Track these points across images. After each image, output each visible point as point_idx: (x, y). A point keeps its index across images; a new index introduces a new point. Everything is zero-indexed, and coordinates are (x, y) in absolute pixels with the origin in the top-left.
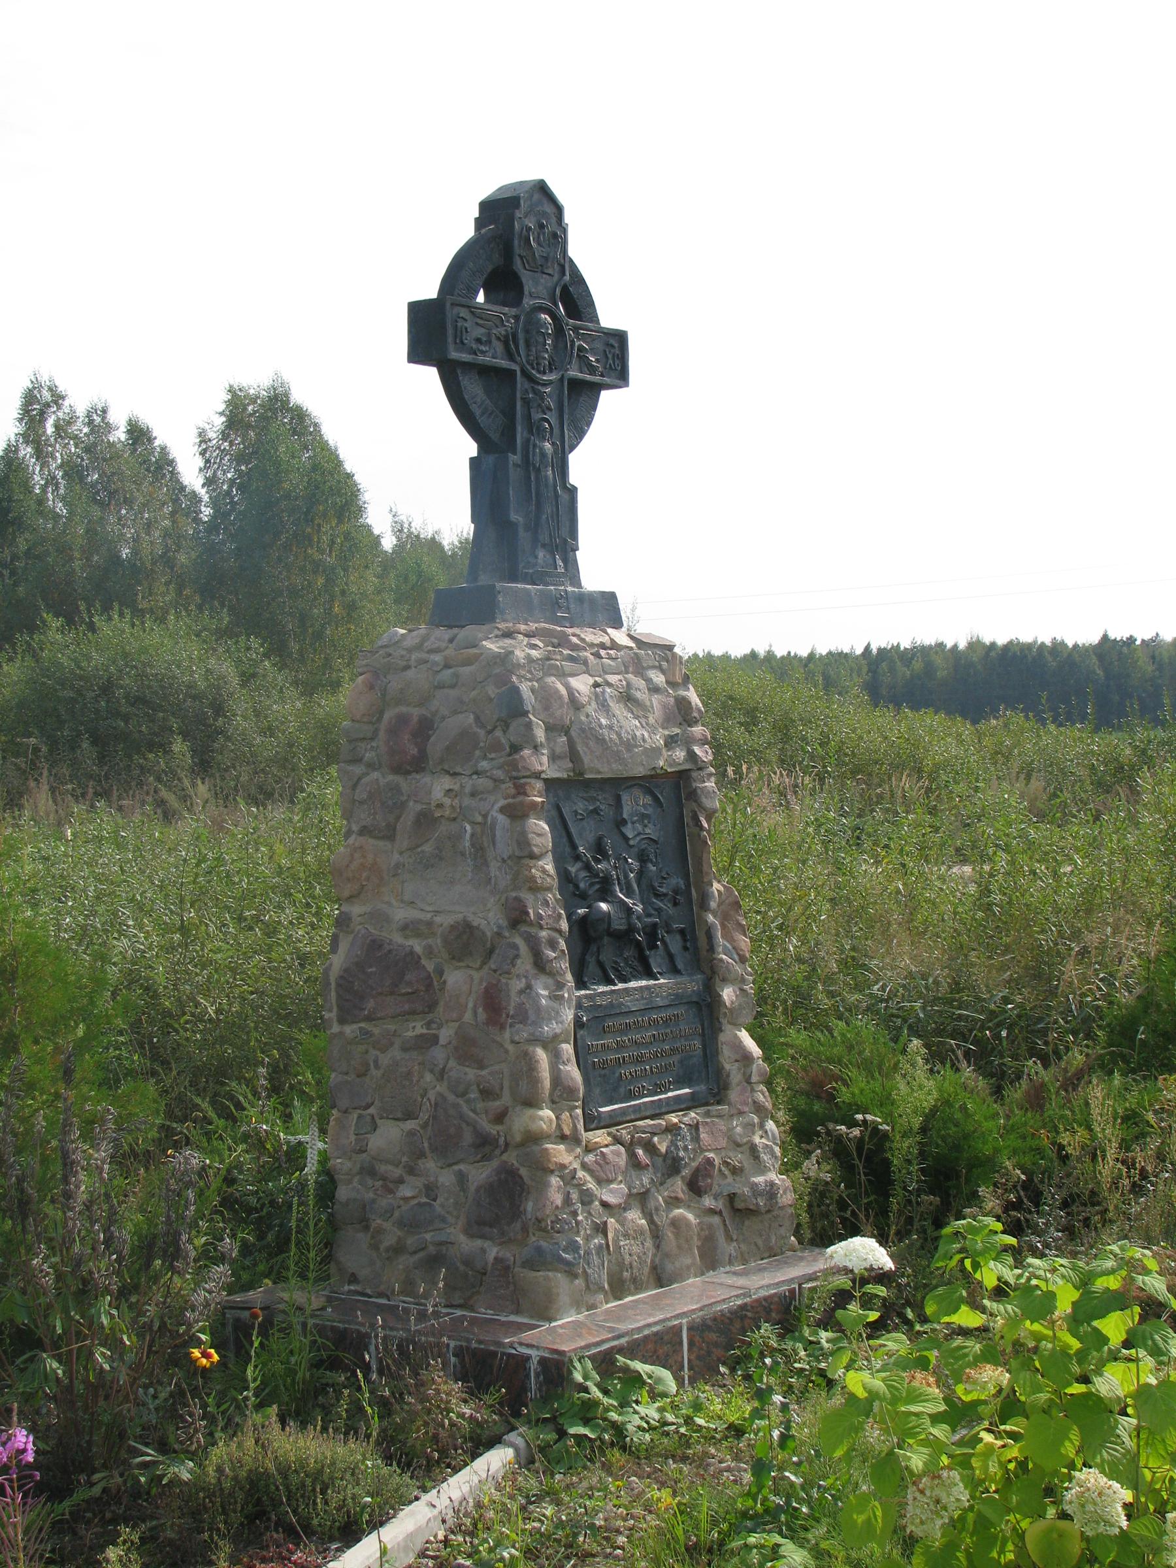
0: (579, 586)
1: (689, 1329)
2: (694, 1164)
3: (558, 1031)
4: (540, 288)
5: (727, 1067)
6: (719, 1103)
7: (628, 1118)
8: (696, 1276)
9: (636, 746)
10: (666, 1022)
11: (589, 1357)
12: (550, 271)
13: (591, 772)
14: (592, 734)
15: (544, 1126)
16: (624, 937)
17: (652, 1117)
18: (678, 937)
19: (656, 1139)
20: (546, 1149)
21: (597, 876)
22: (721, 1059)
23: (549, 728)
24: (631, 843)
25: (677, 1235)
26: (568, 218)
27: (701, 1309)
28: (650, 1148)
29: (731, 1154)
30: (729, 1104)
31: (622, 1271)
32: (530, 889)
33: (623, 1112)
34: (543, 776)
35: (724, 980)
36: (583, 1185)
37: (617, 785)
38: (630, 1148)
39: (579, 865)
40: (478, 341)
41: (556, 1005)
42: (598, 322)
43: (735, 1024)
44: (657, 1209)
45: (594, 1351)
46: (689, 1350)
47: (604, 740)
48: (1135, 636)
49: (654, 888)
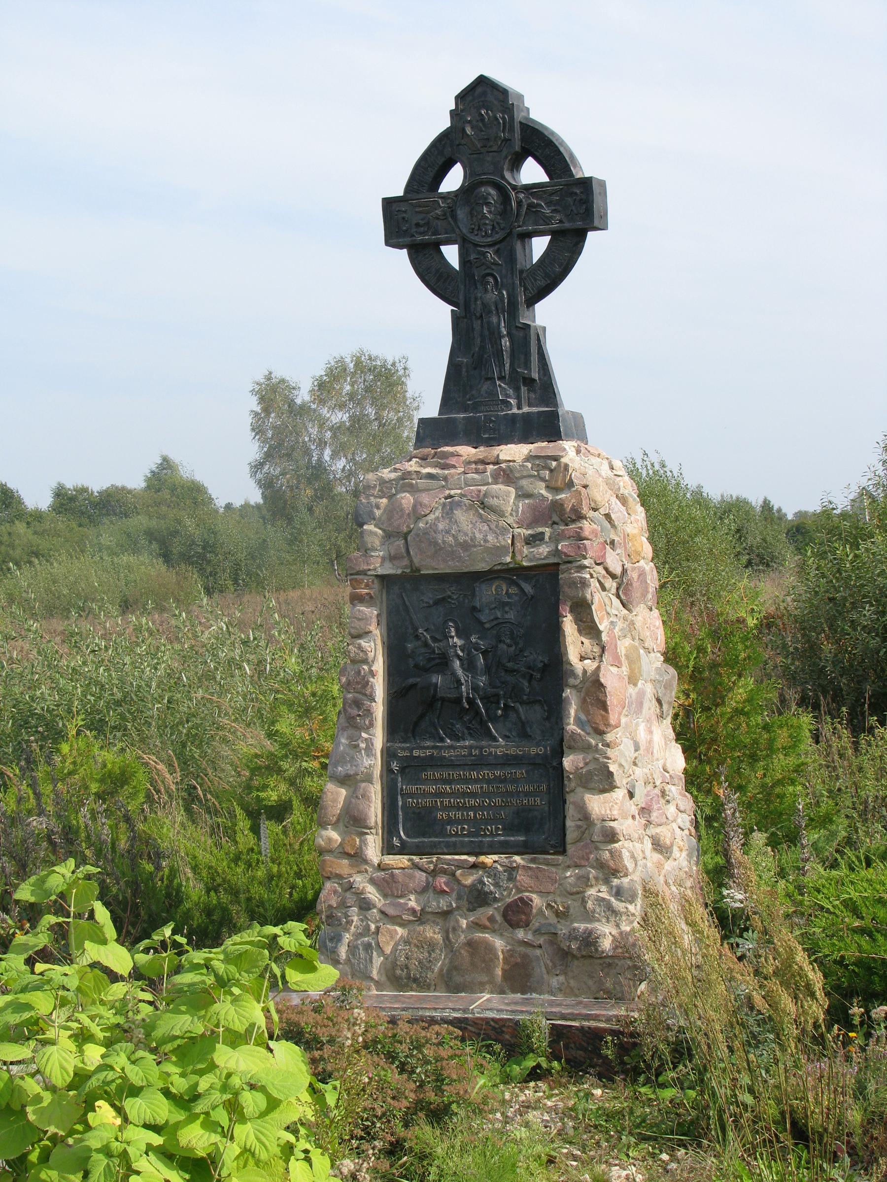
2: (509, 900)
7: (439, 851)
9: (475, 546)
10: (502, 780)
13: (428, 569)
14: (427, 538)
19: (459, 872)
20: (324, 861)
21: (434, 651)
23: (388, 536)
25: (472, 955)
29: (558, 899)
33: (434, 845)
34: (370, 573)
36: (362, 893)
40: (417, 225)
41: (351, 752)
43: (585, 787)
47: (436, 544)
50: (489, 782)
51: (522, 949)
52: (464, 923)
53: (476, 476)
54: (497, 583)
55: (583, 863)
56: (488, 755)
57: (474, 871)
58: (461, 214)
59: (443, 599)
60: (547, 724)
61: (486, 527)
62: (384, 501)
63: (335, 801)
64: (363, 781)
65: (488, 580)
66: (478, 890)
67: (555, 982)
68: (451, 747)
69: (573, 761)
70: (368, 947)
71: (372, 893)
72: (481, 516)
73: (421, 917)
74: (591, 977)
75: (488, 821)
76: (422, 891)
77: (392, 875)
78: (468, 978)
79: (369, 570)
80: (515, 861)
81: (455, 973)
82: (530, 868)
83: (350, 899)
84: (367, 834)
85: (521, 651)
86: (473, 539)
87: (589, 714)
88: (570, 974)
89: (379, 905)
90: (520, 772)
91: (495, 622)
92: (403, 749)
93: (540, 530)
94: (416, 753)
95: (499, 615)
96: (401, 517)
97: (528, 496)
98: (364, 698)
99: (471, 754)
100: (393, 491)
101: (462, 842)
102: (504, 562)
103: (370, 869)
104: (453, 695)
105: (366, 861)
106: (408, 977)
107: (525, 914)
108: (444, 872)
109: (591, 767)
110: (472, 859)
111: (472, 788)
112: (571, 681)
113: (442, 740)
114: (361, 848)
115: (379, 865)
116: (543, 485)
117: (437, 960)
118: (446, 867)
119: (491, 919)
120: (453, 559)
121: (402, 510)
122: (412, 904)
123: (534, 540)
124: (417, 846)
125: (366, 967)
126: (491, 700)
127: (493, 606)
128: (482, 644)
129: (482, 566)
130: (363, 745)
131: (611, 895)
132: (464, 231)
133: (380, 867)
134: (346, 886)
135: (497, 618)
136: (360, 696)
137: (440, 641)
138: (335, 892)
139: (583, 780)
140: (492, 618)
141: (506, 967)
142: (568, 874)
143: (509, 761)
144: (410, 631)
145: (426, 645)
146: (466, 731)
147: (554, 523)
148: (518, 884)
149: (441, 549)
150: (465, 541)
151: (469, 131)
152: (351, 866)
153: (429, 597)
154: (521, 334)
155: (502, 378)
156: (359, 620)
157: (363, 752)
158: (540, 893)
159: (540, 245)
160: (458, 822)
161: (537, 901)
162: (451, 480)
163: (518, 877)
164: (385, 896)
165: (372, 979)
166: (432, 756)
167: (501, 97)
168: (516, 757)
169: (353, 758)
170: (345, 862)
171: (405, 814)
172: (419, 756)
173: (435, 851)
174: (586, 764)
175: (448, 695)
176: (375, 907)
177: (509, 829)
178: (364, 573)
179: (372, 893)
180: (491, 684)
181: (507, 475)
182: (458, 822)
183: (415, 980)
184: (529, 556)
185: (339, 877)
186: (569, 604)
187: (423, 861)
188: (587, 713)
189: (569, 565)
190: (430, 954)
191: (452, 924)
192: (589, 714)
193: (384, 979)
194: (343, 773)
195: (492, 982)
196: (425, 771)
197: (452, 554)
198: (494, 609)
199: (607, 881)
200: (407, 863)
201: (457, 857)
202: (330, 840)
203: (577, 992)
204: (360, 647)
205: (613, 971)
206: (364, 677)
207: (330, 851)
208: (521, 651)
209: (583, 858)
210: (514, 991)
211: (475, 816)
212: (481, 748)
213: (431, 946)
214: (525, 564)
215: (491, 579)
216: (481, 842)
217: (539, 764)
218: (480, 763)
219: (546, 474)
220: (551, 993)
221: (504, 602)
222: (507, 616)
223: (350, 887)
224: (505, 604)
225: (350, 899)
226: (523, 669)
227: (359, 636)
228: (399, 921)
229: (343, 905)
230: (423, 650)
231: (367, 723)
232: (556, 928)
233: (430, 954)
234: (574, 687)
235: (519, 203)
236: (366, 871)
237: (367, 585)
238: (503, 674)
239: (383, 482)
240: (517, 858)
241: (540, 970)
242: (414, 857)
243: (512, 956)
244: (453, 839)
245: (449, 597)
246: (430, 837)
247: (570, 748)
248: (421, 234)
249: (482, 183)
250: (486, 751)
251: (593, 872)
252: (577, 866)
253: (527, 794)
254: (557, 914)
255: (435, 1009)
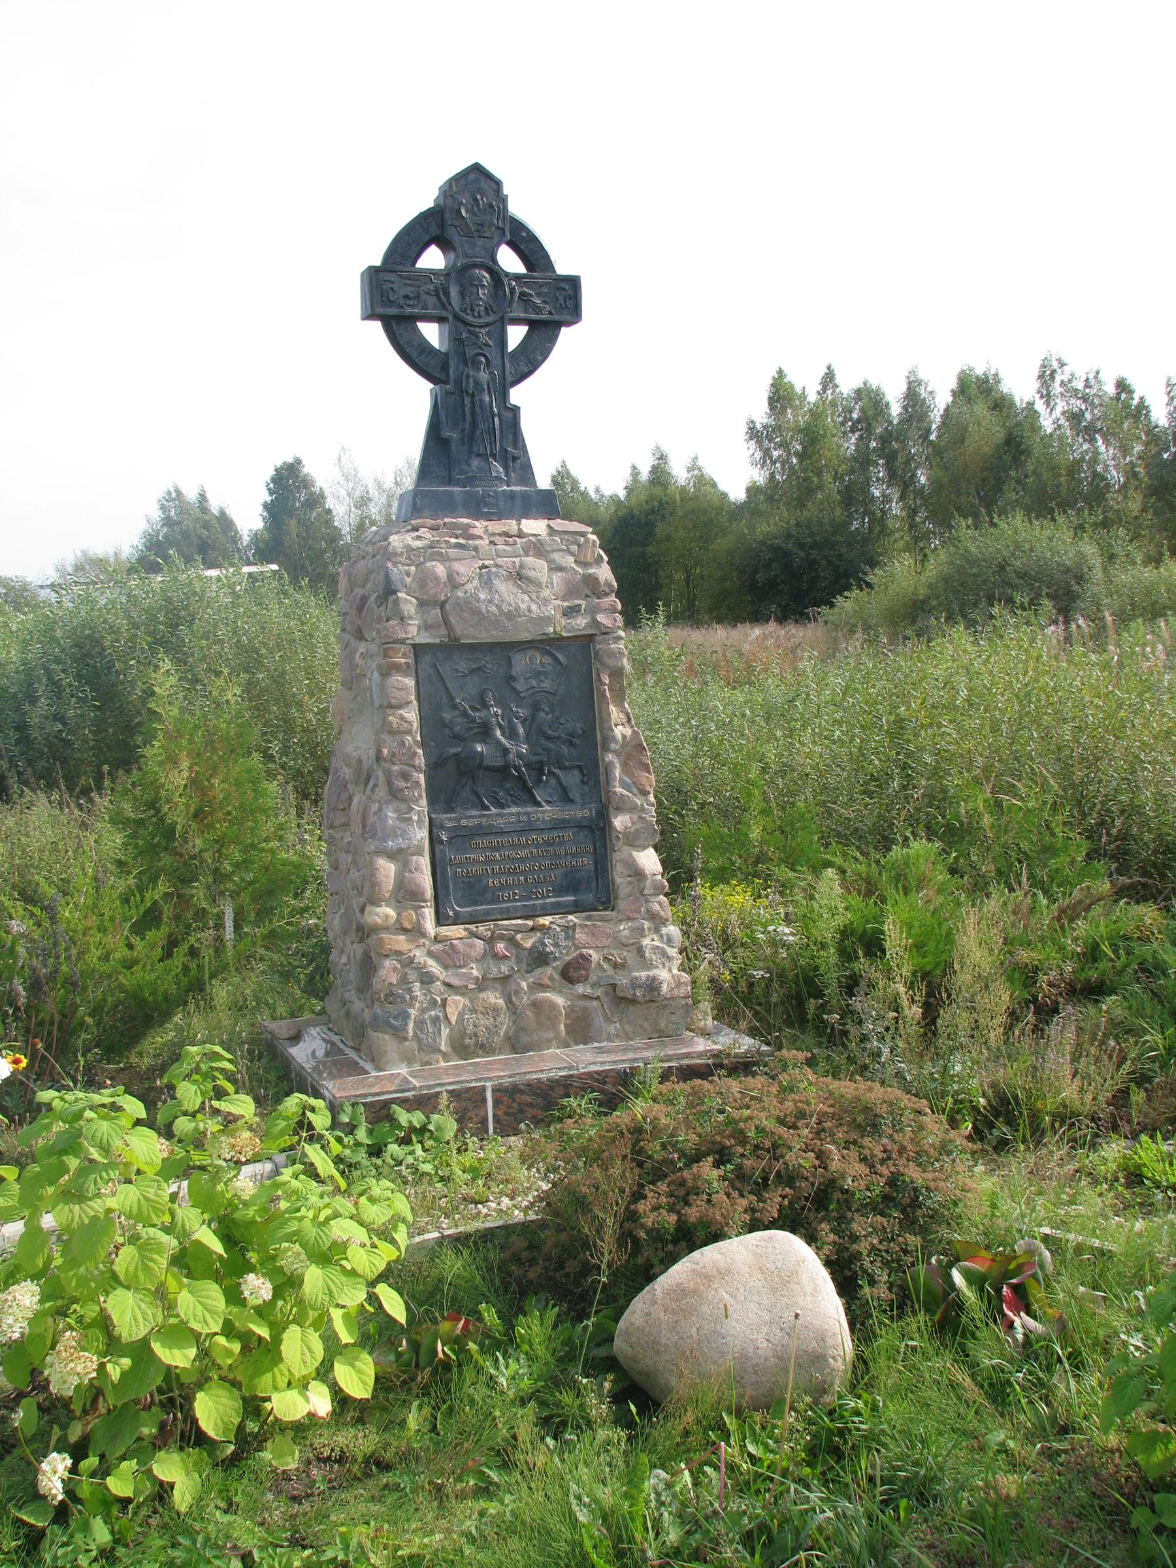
0: (535, 485)
1: (493, 1090)
2: (568, 958)
3: (404, 846)
4: (478, 249)
5: (618, 880)
6: (606, 909)
8: (558, 1048)
9: (520, 616)
10: (548, 843)
11: (364, 1104)
12: (488, 234)
13: (468, 638)
14: (469, 607)
15: (379, 921)
16: (503, 771)
18: (576, 772)
19: (519, 936)
20: (381, 938)
22: (615, 873)
23: (422, 604)
24: (522, 695)
25: (537, 1014)
26: (506, 190)
27: (510, 1076)
28: (512, 941)
29: (615, 952)
30: (619, 911)
31: (463, 1038)
32: (389, 732)
33: (488, 912)
34: (408, 642)
35: (619, 809)
36: (425, 967)
37: (507, 649)
38: (491, 941)
39: (456, 713)
40: (406, 297)
41: (403, 826)
42: (554, 271)
43: (632, 846)
44: (517, 992)
45: (370, 1099)
46: (494, 1107)
47: (480, 612)
48: (262, 501)
49: (544, 733)
50: (537, 846)
51: (582, 1003)
52: (524, 985)
53: (507, 548)
57: (532, 934)
58: (454, 292)
59: (479, 669)
60: (586, 788)
61: (526, 598)
62: (413, 568)
63: (387, 876)
64: (414, 854)
66: (540, 953)
67: (612, 1029)
70: (436, 1020)
71: (434, 967)
72: (521, 588)
73: (482, 984)
74: (647, 1020)
75: (538, 883)
76: (481, 959)
77: (452, 946)
78: (535, 1037)
81: (522, 1034)
82: (586, 926)
83: (412, 975)
86: (517, 609)
88: (625, 1020)
89: (442, 978)
90: (567, 834)
92: (449, 819)
93: (577, 602)
94: (464, 822)
95: (535, 683)
96: (437, 585)
97: (560, 569)
99: (519, 821)
100: (422, 559)
101: (515, 907)
104: (499, 763)
105: (423, 934)
106: (476, 1045)
107: (585, 970)
108: (502, 937)
109: (638, 826)
110: (530, 923)
111: (523, 853)
112: (613, 746)
113: (487, 808)
115: (435, 938)
116: (572, 559)
117: (502, 1023)
119: (551, 978)
120: (496, 629)
121: (437, 578)
122: (475, 973)
123: (570, 612)
124: (470, 914)
125: (434, 1040)
126: (538, 768)
128: (522, 712)
129: (525, 636)
130: (415, 818)
131: (663, 942)
132: (457, 308)
133: (437, 939)
134: (407, 962)
138: (395, 969)
141: (569, 1022)
143: (558, 825)
144: (445, 700)
145: (465, 714)
147: (587, 596)
149: (485, 618)
150: (509, 611)
151: (463, 211)
153: (463, 666)
154: (510, 415)
155: (494, 456)
156: (399, 689)
158: (596, 948)
159: (516, 335)
160: (509, 887)
161: (595, 956)
162: (481, 550)
164: (446, 967)
165: (440, 1051)
166: (480, 825)
167: (495, 187)
168: (563, 821)
169: (405, 831)
170: (402, 938)
171: (456, 884)
174: (633, 823)
176: (438, 979)
177: (560, 891)
178: (402, 642)
179: (434, 967)
180: (532, 751)
181: (537, 548)
182: (509, 887)
183: (482, 1046)
184: (562, 626)
185: (399, 953)
187: (482, 929)
188: (631, 775)
190: (495, 1019)
191: (513, 987)
193: (450, 1050)
194: (395, 848)
195: (557, 1037)
197: (497, 624)
199: (657, 930)
200: (464, 933)
201: (514, 922)
202: (387, 916)
203: (631, 1035)
204: (402, 718)
205: (667, 1011)
206: (410, 748)
207: (386, 929)
209: (635, 911)
210: (577, 1044)
211: (526, 880)
212: (528, 814)
213: (496, 1010)
214: (564, 634)
218: (528, 829)
219: (574, 548)
220: (609, 1039)
223: (411, 961)
224: (539, 673)
225: (412, 975)
227: (400, 707)
228: (464, 990)
229: (404, 980)
230: (460, 720)
232: (614, 979)
233: (495, 1019)
234: (615, 752)
235: (512, 291)
236: (424, 945)
239: (409, 549)
240: (571, 917)
241: (598, 1020)
243: (572, 1011)
244: (506, 905)
247: (617, 809)
248: (410, 306)
249: (475, 266)
251: (646, 924)
252: (629, 919)
253: (574, 855)
254: (615, 966)
255: (542, 1071)
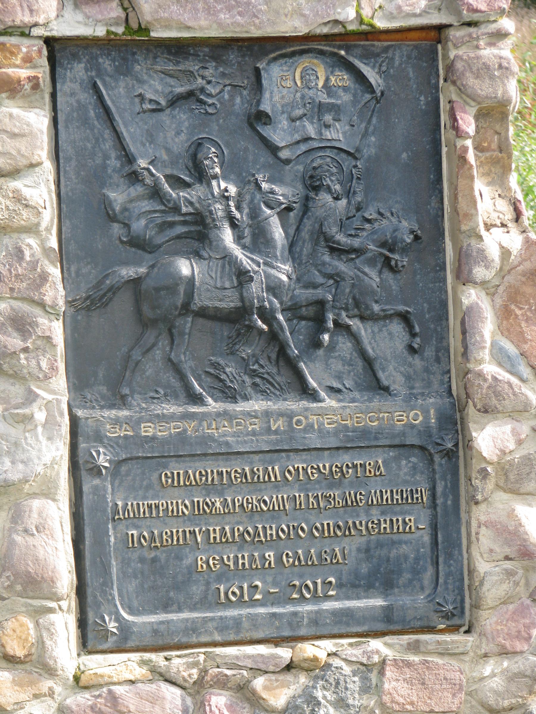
6: (454, 629)
7: (204, 639)
13: (168, 27)
17: (277, 642)
21: (176, 209)
24: (284, 154)
34: (36, 32)
43: (515, 492)
49: (328, 239)
54: (305, 62)
55: (519, 646)
56: (305, 430)
57: (289, 677)
59: (190, 94)
60: (417, 362)
64: (34, 495)
65: (283, 56)
68: (225, 415)
69: (494, 439)
79: (36, 25)
80: (378, 652)
82: (409, 664)
84: (51, 610)
85: (358, 209)
87: (525, 341)
91: (303, 147)
95: (311, 130)
98: (37, 311)
101: (252, 618)
102: (341, 18)
103: (58, 689)
113: (197, 399)
114: (41, 642)
118: (229, 672)
127: (298, 112)
135: (307, 139)
136: (25, 307)
137: (188, 185)
139: (512, 477)
140: (297, 137)
142: (487, 670)
144: (114, 163)
146: (247, 379)
148: (386, 699)
152: (18, 683)
156: (14, 136)
157: (40, 429)
163: (386, 686)
166: (182, 436)
168: (365, 433)
171: (125, 563)
172: (154, 438)
173: (194, 640)
174: (520, 442)
175: (218, 304)
186: (473, 111)
189: (472, 30)
192: (525, 341)
196: (165, 467)
198: (300, 118)
208: (358, 209)
209: (519, 636)
211: (279, 559)
212: (289, 416)
215: (293, 54)
216: (295, 614)
217: (412, 446)
221: (320, 105)
222: (328, 134)
226: (371, 247)
230: (146, 205)
231: (44, 364)
234: (483, 284)
236: (51, 693)
237: (28, 60)
238: (327, 258)
240: (375, 644)
242: (152, 656)
245: (202, 90)
246: (180, 610)
247: (486, 411)
250: (299, 422)
